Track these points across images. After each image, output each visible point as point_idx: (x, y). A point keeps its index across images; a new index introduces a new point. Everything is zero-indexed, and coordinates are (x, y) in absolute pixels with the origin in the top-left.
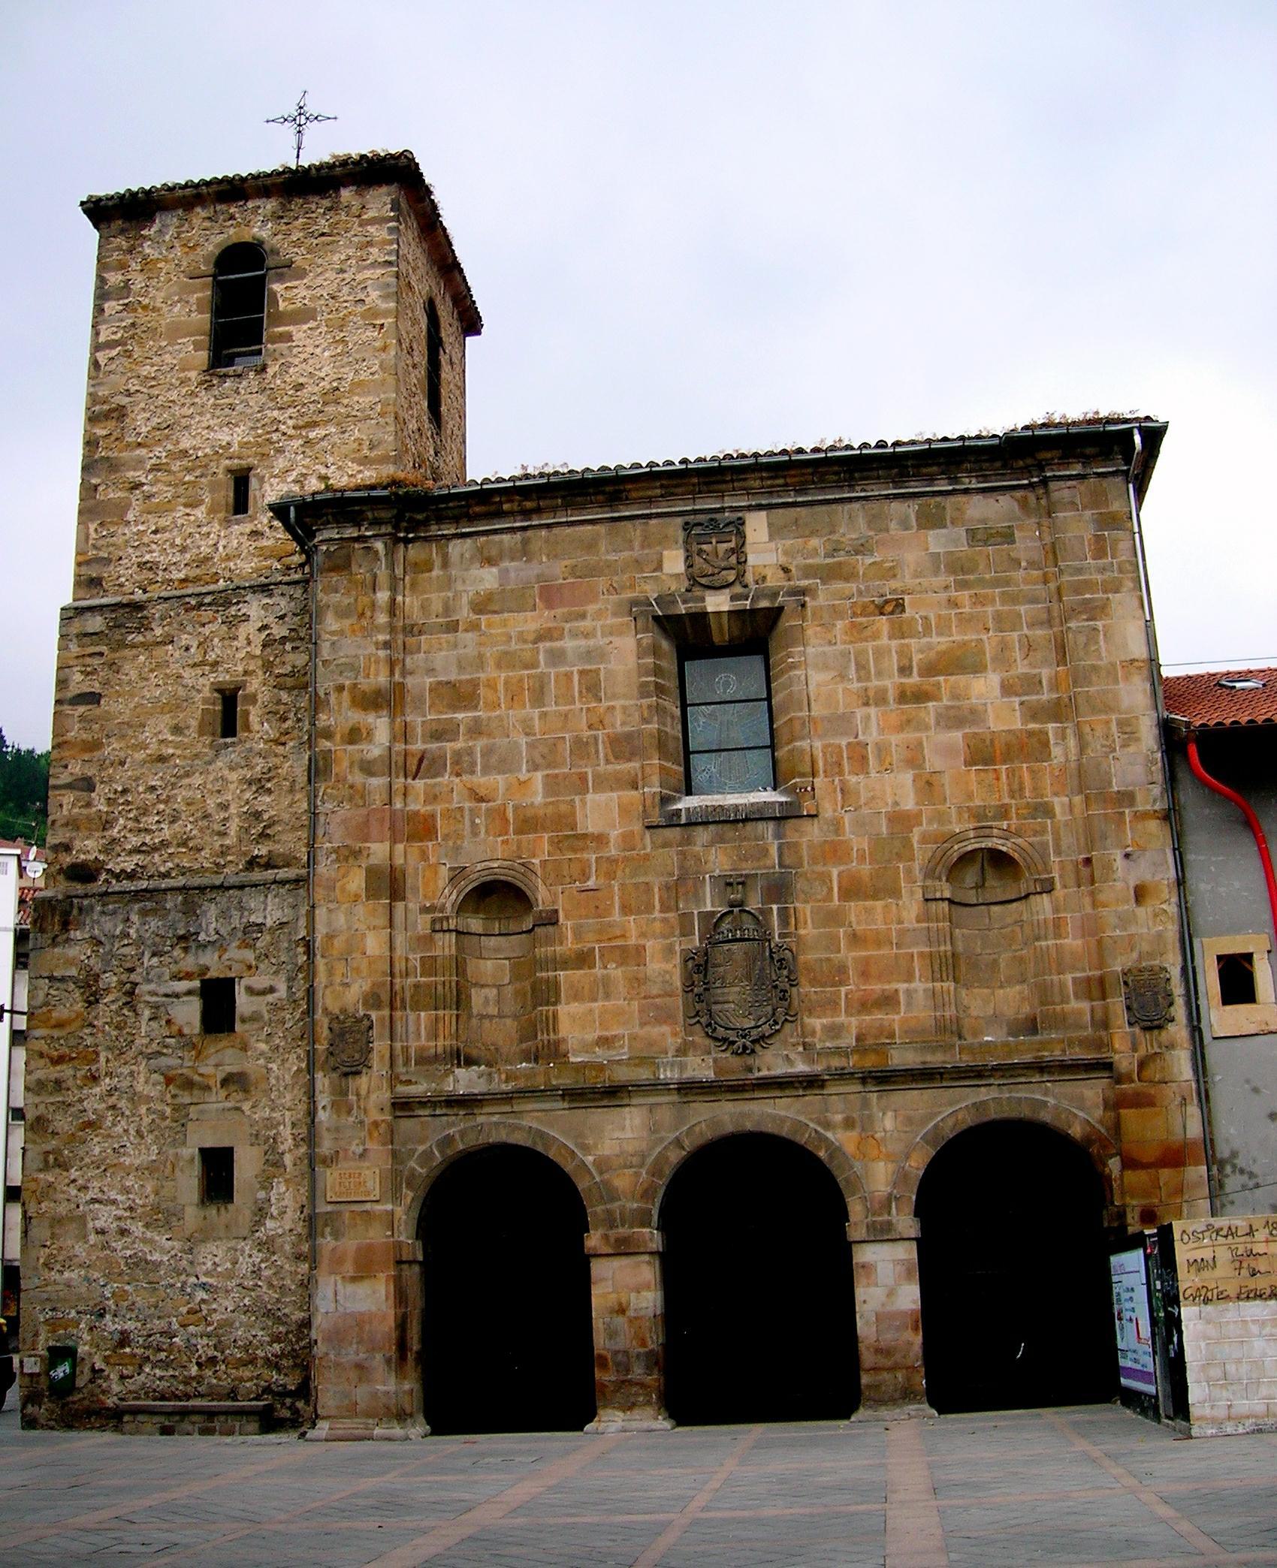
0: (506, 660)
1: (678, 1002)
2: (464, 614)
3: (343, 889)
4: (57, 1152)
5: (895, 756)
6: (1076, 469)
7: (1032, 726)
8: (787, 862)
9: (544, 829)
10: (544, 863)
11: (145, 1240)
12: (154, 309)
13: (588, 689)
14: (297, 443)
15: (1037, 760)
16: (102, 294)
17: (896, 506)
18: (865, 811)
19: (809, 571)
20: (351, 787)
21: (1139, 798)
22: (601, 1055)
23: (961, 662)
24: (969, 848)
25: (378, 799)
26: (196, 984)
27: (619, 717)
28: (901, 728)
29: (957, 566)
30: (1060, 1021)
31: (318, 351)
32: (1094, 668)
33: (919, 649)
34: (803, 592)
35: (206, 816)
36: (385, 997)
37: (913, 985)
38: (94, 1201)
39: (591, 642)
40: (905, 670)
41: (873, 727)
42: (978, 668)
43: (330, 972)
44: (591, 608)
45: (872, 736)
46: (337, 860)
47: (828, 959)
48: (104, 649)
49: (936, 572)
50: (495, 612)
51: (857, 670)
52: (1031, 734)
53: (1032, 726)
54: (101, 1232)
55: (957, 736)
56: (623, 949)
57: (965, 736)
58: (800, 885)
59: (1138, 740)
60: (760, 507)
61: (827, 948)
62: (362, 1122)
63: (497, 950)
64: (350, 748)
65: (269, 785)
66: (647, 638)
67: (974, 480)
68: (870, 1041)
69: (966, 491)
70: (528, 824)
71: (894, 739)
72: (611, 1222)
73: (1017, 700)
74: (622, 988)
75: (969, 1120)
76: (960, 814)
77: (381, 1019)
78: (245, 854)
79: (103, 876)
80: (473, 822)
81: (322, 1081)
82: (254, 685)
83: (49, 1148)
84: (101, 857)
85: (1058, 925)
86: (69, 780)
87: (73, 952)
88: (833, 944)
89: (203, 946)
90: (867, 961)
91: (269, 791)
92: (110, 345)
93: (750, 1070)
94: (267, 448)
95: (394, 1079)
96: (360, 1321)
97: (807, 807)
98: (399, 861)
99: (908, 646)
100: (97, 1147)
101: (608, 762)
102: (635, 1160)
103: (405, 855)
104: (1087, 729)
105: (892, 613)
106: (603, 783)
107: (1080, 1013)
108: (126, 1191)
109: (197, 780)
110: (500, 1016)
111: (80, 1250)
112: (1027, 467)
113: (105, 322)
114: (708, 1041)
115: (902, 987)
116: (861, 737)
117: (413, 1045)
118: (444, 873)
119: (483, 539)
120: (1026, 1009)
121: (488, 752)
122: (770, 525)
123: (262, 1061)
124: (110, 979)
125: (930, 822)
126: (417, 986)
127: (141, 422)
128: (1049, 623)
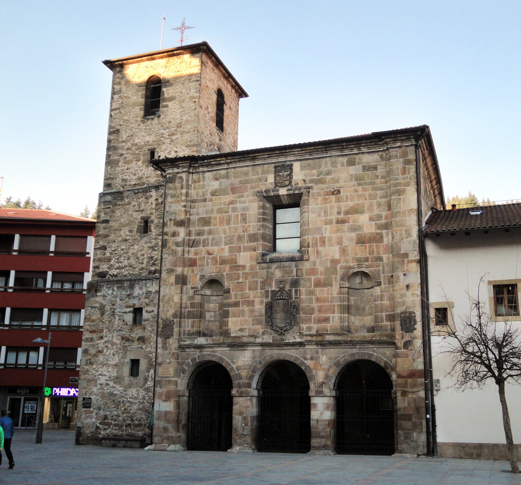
0: (220, 211)
1: (264, 318)
2: (208, 196)
3: (168, 282)
4: (90, 359)
5: (334, 241)
6: (399, 144)
7: (378, 231)
8: (299, 275)
9: (228, 263)
10: (227, 274)
11: (113, 387)
12: (129, 97)
13: (243, 220)
14: (168, 141)
15: (379, 242)
16: (113, 93)
17: (340, 159)
18: (323, 259)
19: (312, 181)
20: (172, 250)
21: (410, 255)
22: (240, 334)
23: (356, 210)
24: (356, 271)
25: (180, 254)
26: (132, 309)
27: (251, 228)
28: (337, 232)
29: (358, 179)
30: (380, 328)
31: (176, 110)
32: (399, 212)
33: (344, 206)
34: (309, 188)
35: (138, 258)
36: (178, 315)
37: (334, 315)
38: (100, 375)
39: (245, 205)
40: (339, 213)
41: (328, 231)
42: (362, 212)
43: (164, 306)
44: (245, 194)
45: (327, 234)
46: (167, 273)
47: (309, 306)
48: (111, 206)
49: (351, 180)
50: (217, 195)
51: (324, 213)
52: (377, 234)
53: (378, 231)
54: (101, 384)
55: (354, 235)
56: (248, 301)
57: (357, 235)
58: (302, 282)
59: (411, 236)
60: (298, 160)
61: (309, 302)
62: (170, 353)
63: (215, 300)
64: (173, 238)
65: (156, 248)
66: (261, 204)
67: (366, 149)
68: (320, 332)
69: (363, 153)
70: (224, 262)
71: (334, 235)
72: (239, 386)
73: (374, 223)
74: (247, 313)
75: (350, 359)
76: (353, 260)
77: (177, 321)
78: (148, 269)
79: (108, 276)
80: (207, 262)
81: (160, 340)
82: (153, 217)
83: (88, 358)
84: (108, 270)
85: (382, 296)
86: (99, 246)
87: (98, 299)
88: (311, 301)
89: (134, 298)
90: (321, 306)
91: (156, 250)
92: (115, 109)
93: (283, 340)
94: (159, 143)
95: (180, 340)
96: (166, 413)
97: (306, 257)
98: (185, 273)
99: (341, 205)
100: (101, 358)
101: (247, 242)
102: (248, 367)
103: (187, 271)
104: (394, 232)
105: (336, 194)
106: (246, 249)
107: (387, 326)
108: (108, 372)
109: (136, 247)
110: (215, 321)
111: (95, 390)
112: (383, 144)
113: (114, 102)
114: (271, 331)
115: (331, 315)
116: (324, 235)
117: (187, 329)
118: (198, 276)
119: (215, 172)
120: (372, 324)
121: (213, 239)
122: (301, 166)
123: (149, 333)
124: (108, 308)
125: (343, 262)
126: (189, 312)
127: (124, 136)
128: (386, 197)
